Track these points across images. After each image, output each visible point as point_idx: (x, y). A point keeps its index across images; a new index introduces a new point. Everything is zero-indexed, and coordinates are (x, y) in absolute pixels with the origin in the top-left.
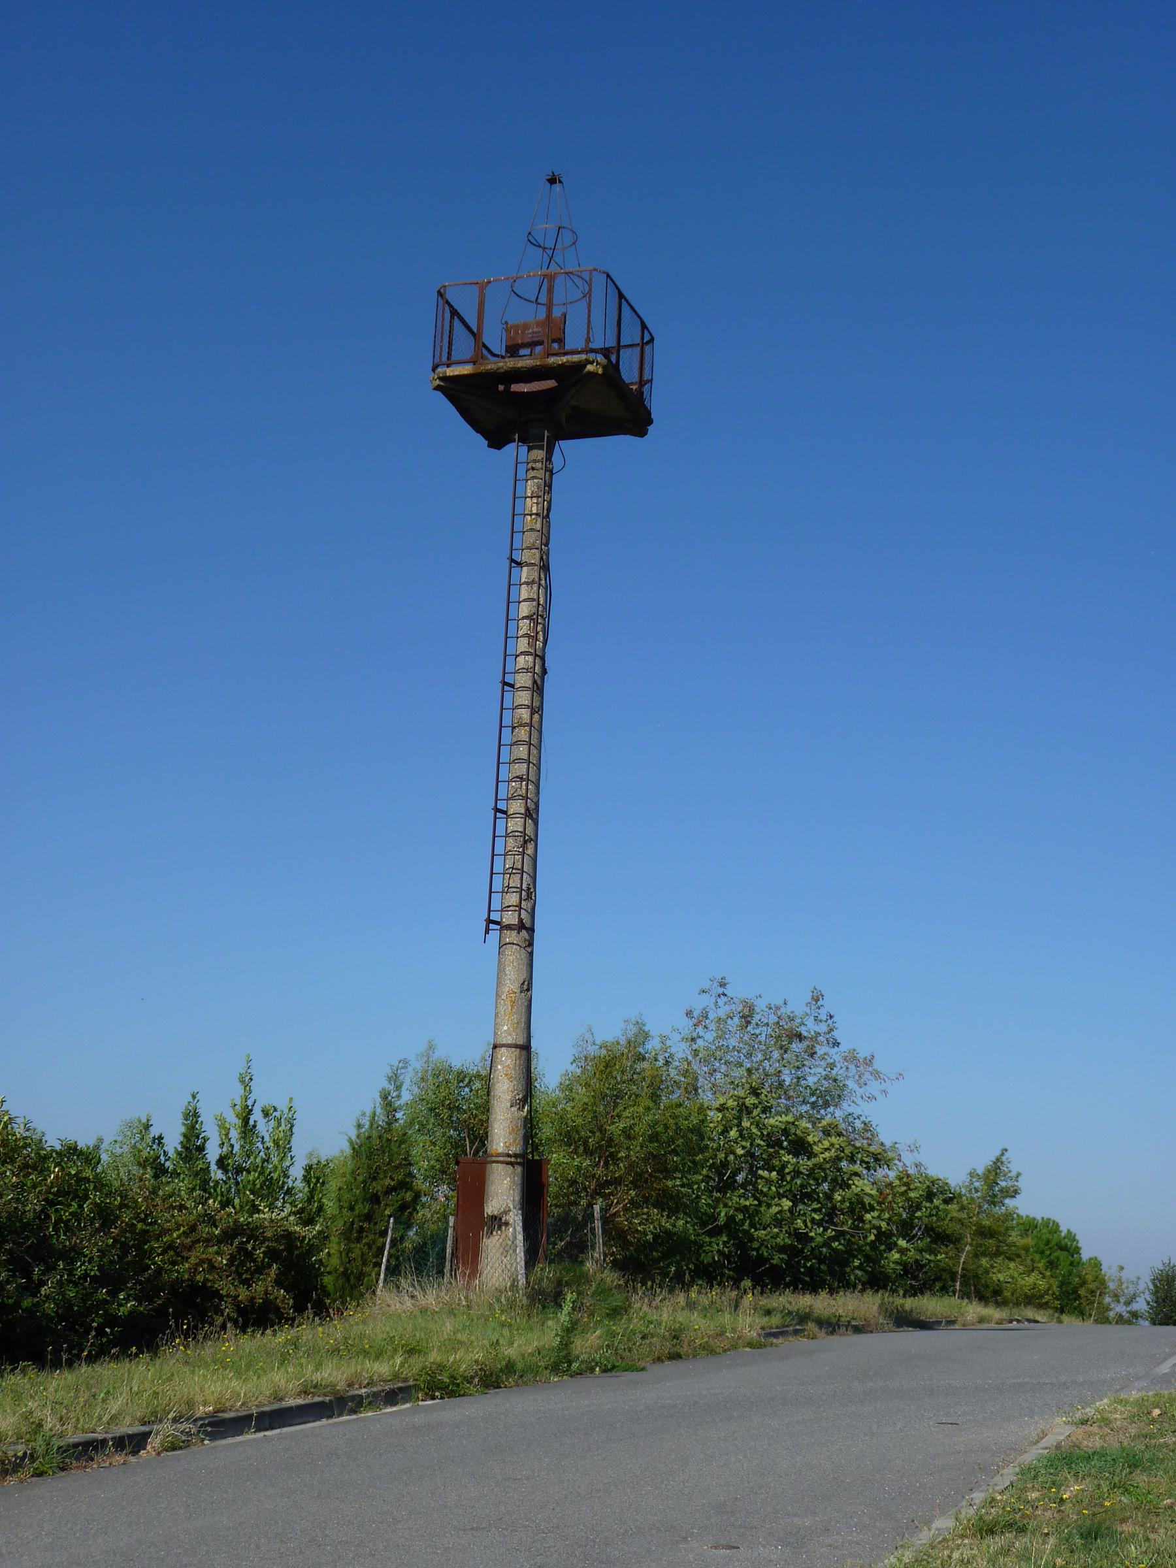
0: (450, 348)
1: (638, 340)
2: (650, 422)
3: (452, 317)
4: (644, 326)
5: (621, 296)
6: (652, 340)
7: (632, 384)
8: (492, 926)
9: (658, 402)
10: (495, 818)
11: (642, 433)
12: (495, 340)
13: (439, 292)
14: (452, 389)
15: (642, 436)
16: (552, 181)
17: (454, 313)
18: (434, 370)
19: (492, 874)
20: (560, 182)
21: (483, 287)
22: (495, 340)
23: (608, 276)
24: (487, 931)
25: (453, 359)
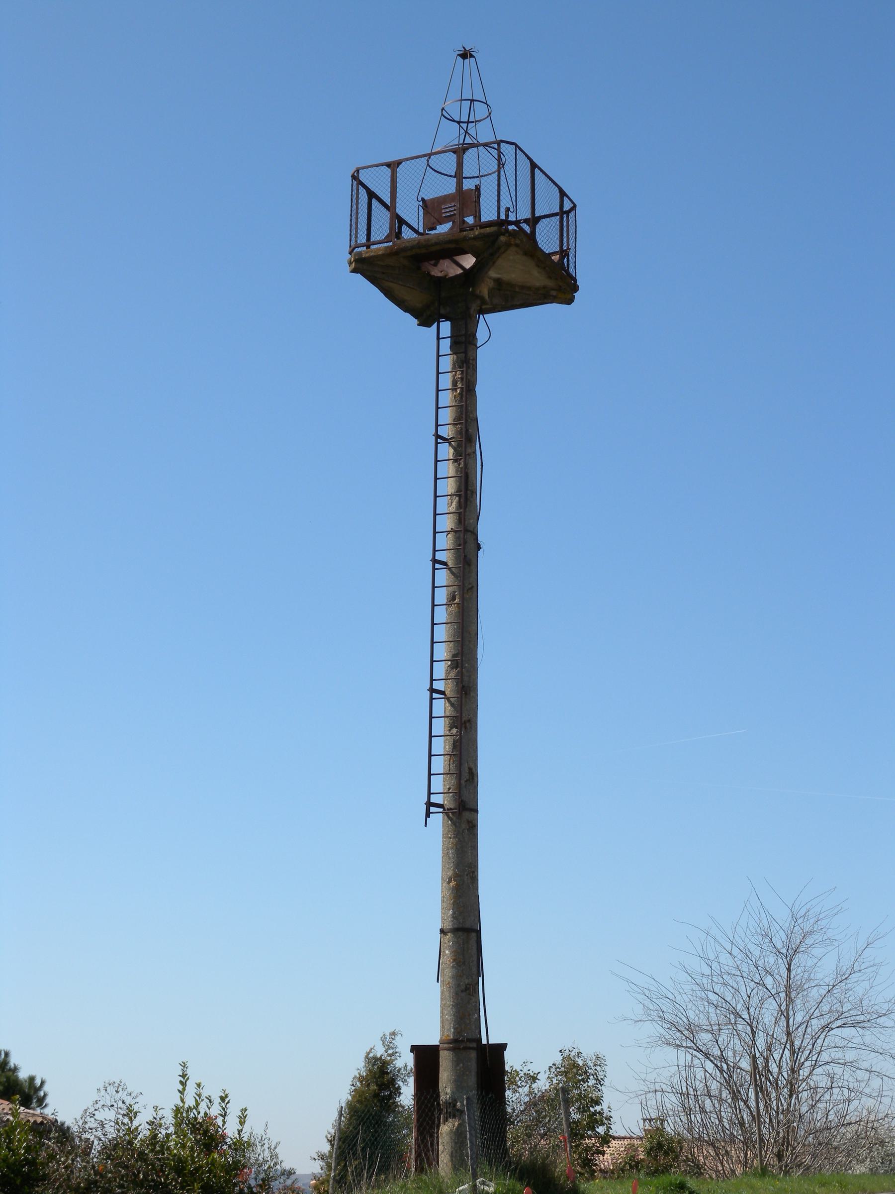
0: (357, 208)
1: (557, 210)
2: (576, 288)
3: (358, 185)
4: (563, 194)
5: (534, 166)
6: (574, 207)
7: (554, 253)
8: (432, 809)
9: (584, 269)
10: (432, 699)
11: (569, 301)
12: (411, 212)
13: (355, 177)
14: (365, 265)
15: (569, 304)
16: (465, 55)
17: (371, 195)
18: (350, 253)
19: (430, 755)
20: (472, 56)
21: (393, 166)
22: (411, 212)
23: (516, 146)
24: (428, 814)
25: (373, 239)
